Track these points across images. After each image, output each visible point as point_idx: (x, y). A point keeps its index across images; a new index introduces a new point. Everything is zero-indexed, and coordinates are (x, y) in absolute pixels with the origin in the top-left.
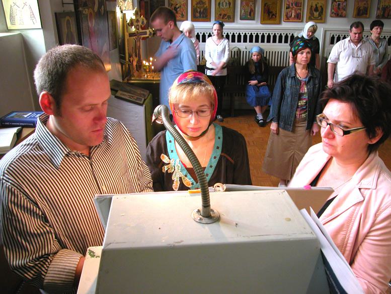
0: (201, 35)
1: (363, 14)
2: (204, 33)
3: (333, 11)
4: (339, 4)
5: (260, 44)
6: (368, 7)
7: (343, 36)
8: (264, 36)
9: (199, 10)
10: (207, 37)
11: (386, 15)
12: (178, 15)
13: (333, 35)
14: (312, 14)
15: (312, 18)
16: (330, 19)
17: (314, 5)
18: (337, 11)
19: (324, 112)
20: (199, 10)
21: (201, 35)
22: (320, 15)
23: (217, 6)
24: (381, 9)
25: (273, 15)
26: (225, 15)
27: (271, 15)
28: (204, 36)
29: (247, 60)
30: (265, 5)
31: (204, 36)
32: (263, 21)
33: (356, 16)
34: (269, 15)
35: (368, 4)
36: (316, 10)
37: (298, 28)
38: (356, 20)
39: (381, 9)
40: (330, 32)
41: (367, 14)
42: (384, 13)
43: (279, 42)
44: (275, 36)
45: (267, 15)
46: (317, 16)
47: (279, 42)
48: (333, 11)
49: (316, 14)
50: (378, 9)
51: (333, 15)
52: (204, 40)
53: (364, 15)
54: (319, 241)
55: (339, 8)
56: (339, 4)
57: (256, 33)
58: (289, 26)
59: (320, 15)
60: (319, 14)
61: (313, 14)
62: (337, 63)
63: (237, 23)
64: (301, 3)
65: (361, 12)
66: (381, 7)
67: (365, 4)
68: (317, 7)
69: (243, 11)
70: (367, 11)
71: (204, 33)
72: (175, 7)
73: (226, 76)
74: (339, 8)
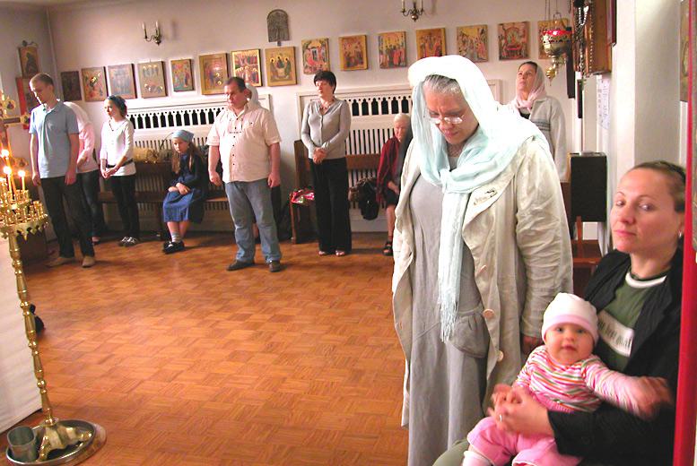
1: (356, 63)
3: (306, 63)
5: (184, 127)
6: (362, 52)
7: (216, 110)
8: (397, 102)
10: (215, 114)
11: (396, 62)
12: (96, 92)
14: (276, 73)
15: (276, 78)
17: (276, 59)
18: (313, 64)
23: (142, 76)
24: (384, 52)
26: (153, 87)
27: (215, 79)
28: (211, 114)
29: (386, 139)
32: (206, 92)
33: (345, 67)
34: (213, 81)
39: (384, 52)
40: (310, 98)
41: (362, 63)
42: (391, 57)
43: (383, 113)
44: (385, 103)
46: (284, 74)
47: (178, 125)
49: (281, 71)
50: (381, 52)
51: (308, 70)
52: (212, 121)
53: (359, 65)
54: (463, 371)
55: (315, 59)
59: (288, 72)
60: (285, 71)
61: (276, 71)
63: (173, 97)
64: (256, 58)
66: (385, 49)
67: (356, 47)
68: (280, 61)
69: (176, 79)
70: (361, 58)
73: (134, 175)
74: (315, 59)
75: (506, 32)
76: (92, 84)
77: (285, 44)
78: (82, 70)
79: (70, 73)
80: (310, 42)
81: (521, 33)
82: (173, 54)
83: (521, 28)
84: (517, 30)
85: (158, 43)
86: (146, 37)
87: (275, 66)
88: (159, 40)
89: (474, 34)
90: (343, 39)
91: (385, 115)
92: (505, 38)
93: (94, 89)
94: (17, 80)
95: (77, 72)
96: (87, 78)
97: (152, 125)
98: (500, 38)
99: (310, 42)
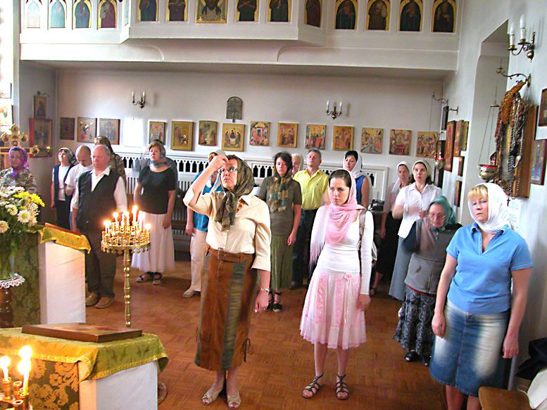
0: (198, 165)
1: (288, 143)
2: (195, 162)
4: (259, 131)
6: (294, 135)
8: (190, 164)
9: (107, 132)
13: (256, 166)
16: (249, 147)
17: (230, 132)
19: (363, 313)
20: (107, 132)
21: (198, 165)
22: (238, 141)
25: (185, 140)
28: (201, 166)
30: (175, 129)
31: (201, 166)
33: (280, 144)
35: (294, 132)
36: (233, 136)
37: (375, 167)
38: (280, 150)
41: (293, 143)
45: (178, 140)
48: (252, 138)
49: (233, 140)
50: (307, 137)
56: (259, 131)
57: (186, 161)
58: (374, 165)
59: (238, 141)
62: (315, 211)
65: (287, 140)
66: (310, 136)
69: (152, 135)
70: (293, 140)
71: (263, 167)
72: (84, 128)
75: (396, 135)
76: (84, 129)
77: (238, 122)
78: (79, 118)
79: (68, 119)
80: (257, 123)
81: (406, 138)
82: (151, 117)
83: (407, 134)
84: (404, 136)
85: (142, 107)
86: (134, 102)
87: (229, 136)
88: (142, 105)
89: (374, 135)
90: (281, 124)
91: (188, 173)
92: (395, 139)
93: (85, 133)
94: (30, 119)
95: (74, 119)
96: (81, 125)
97: (394, 18)
98: (392, 139)
99: (257, 123)
